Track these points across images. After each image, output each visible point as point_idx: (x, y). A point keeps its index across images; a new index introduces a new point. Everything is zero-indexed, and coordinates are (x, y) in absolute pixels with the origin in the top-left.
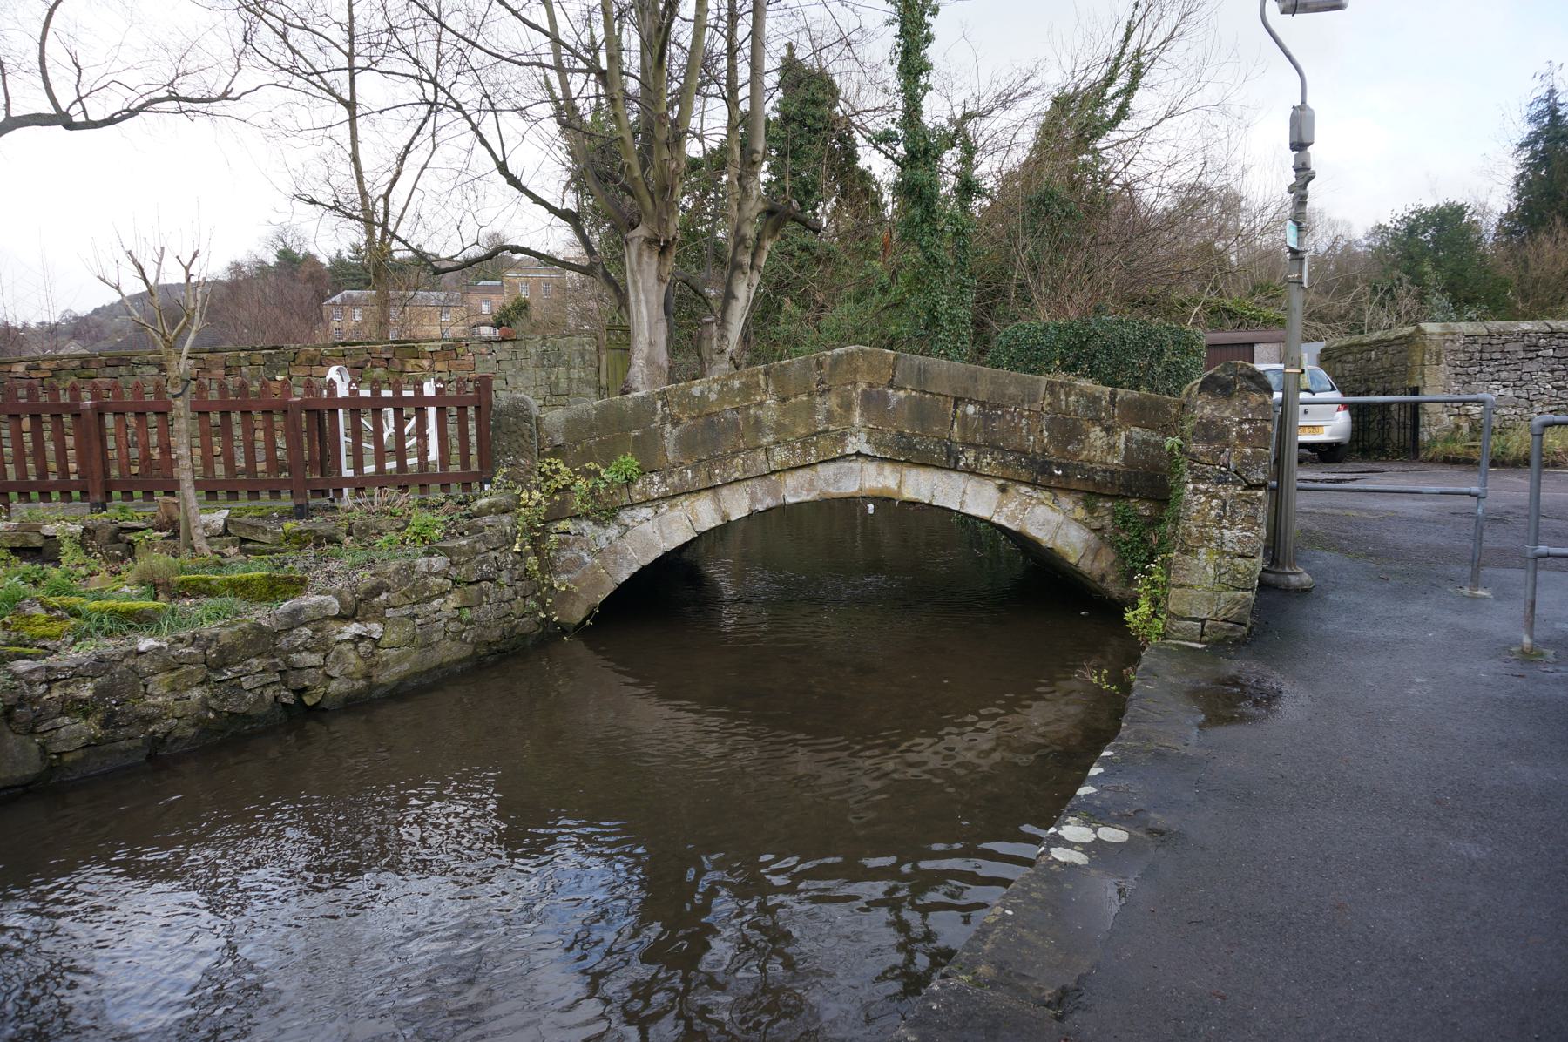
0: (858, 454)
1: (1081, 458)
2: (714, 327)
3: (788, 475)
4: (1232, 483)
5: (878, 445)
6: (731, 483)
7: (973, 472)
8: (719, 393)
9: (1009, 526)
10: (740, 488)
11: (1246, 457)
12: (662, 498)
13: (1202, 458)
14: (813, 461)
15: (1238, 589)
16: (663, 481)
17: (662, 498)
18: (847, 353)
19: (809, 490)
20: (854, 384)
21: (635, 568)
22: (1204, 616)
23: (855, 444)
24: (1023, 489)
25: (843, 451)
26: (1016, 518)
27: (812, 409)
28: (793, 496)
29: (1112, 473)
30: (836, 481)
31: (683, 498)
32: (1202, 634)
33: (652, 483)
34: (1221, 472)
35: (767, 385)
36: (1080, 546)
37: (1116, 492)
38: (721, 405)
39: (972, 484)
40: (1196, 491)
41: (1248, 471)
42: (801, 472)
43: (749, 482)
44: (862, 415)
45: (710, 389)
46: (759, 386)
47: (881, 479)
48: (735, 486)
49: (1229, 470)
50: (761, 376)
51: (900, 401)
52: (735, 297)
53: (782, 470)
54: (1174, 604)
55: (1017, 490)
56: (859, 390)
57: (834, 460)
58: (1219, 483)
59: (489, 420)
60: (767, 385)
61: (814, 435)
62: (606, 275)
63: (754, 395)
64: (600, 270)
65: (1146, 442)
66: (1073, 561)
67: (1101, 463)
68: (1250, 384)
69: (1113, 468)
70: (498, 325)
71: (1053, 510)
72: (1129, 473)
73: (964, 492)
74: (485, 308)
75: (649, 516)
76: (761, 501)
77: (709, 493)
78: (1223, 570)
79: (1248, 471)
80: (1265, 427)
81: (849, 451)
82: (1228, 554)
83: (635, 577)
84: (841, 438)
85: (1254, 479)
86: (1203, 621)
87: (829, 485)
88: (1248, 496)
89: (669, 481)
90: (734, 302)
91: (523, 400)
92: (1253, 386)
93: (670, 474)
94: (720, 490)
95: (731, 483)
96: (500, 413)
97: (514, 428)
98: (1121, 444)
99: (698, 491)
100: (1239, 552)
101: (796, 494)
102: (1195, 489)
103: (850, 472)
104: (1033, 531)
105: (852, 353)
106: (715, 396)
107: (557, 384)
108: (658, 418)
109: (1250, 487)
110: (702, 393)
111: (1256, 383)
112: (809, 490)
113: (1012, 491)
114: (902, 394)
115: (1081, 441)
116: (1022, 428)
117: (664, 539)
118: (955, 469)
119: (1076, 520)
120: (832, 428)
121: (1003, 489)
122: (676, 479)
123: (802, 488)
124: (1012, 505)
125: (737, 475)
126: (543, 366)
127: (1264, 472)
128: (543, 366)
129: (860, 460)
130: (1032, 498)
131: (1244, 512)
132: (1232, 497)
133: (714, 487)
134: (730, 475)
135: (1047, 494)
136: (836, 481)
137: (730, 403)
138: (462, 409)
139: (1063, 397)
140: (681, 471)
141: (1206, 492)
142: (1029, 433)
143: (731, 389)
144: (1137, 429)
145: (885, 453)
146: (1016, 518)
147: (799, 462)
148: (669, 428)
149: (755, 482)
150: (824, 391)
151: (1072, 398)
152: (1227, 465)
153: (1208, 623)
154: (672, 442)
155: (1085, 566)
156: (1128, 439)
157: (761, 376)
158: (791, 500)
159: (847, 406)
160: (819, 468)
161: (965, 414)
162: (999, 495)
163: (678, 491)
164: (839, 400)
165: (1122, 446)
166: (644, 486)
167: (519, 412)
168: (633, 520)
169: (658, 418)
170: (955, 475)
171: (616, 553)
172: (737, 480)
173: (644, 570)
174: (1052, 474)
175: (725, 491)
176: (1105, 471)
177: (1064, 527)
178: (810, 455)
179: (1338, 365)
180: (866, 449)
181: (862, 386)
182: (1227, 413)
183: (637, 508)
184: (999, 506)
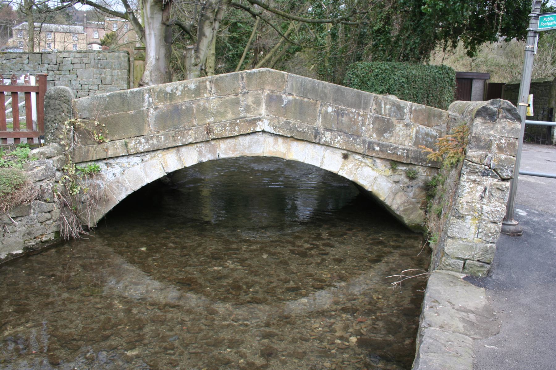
0: (263, 131)
1: (391, 141)
2: (193, 52)
3: (221, 141)
4: (492, 177)
5: (275, 127)
6: (187, 145)
7: (327, 145)
8: (182, 91)
9: (348, 178)
10: (192, 148)
11: (502, 161)
12: (147, 152)
13: (474, 159)
14: (236, 134)
15: (488, 242)
16: (147, 142)
17: (147, 152)
18: (259, 72)
19: (233, 151)
20: (263, 90)
21: (129, 192)
22: (466, 257)
23: (264, 125)
24: (357, 157)
25: (254, 129)
26: (352, 173)
27: (237, 103)
28: (224, 154)
29: (408, 150)
30: (250, 147)
31: (159, 152)
32: (464, 268)
33: (140, 143)
34: (485, 169)
35: (211, 88)
36: (386, 190)
37: (409, 162)
38: (183, 99)
39: (328, 152)
40: (469, 180)
41: (502, 170)
42: (229, 140)
43: (198, 145)
44: (266, 109)
45: (177, 89)
46: (206, 88)
47: (276, 147)
48: (190, 147)
49: (490, 168)
50: (208, 82)
51: (289, 102)
52: (204, 35)
53: (218, 139)
54: (448, 249)
55: (354, 157)
56: (266, 94)
57: (249, 134)
58: (483, 176)
59: (43, 101)
60: (211, 88)
61: (238, 119)
62: (135, 20)
63: (203, 93)
64: (131, 17)
65: (427, 134)
66: (382, 199)
67: (402, 144)
68: (508, 114)
69: (408, 148)
70: (103, 43)
71: (373, 169)
72: (417, 151)
73: (323, 158)
74: (96, 36)
75: (138, 162)
76: (205, 156)
77: (174, 150)
78: (480, 230)
79: (502, 170)
80: (515, 143)
81: (258, 129)
82: (485, 220)
83: (129, 197)
84: (254, 121)
85: (505, 175)
86: (465, 260)
87: (245, 149)
88: (501, 185)
89: (151, 142)
90: (204, 38)
91: (64, 90)
92: (510, 116)
93: (152, 138)
94: (180, 149)
95: (187, 145)
96: (50, 97)
97: (58, 107)
98: (413, 134)
99: (168, 148)
100: (492, 220)
101: (226, 153)
102: (468, 178)
103: (258, 141)
104: (361, 181)
105: (263, 72)
106: (180, 93)
107: (105, 79)
108: (146, 104)
109: (503, 180)
110: (172, 90)
111: (512, 115)
112: (233, 151)
113: (351, 158)
114: (290, 98)
115: (391, 132)
116: (359, 122)
117: (147, 175)
118: (319, 144)
119: (385, 176)
120: (248, 115)
121: (345, 157)
122: (155, 141)
123: (230, 149)
124: (350, 166)
125: (191, 140)
126: (98, 68)
127: (512, 171)
128: (98, 68)
129: (264, 135)
130: (362, 162)
131: (498, 194)
132: (491, 185)
133: (178, 147)
134: (187, 140)
135: (370, 160)
136: (250, 147)
137: (189, 97)
138: (28, 94)
139: (383, 106)
140: (158, 137)
141: (474, 181)
142: (362, 125)
143: (189, 89)
144: (423, 127)
145: (279, 131)
146: (352, 173)
147: (228, 134)
148: (152, 110)
149: (201, 145)
150: (245, 93)
151: (388, 107)
152: (489, 165)
153: (468, 262)
154: (154, 119)
155: (388, 202)
156: (417, 132)
157: (208, 82)
158: (222, 156)
159: (258, 103)
160: (240, 138)
161: (326, 112)
162: (343, 160)
163: (156, 148)
164: (253, 99)
165: (414, 136)
166: (136, 144)
167: (62, 97)
168: (129, 163)
169: (146, 104)
170: (318, 147)
171: (118, 182)
172: (191, 144)
173: (148, 185)
174: (374, 149)
175: (183, 149)
176: (403, 149)
177: (378, 179)
178: (235, 130)
179: (513, 93)
180: (267, 129)
181: (267, 92)
182: (492, 132)
183: (131, 157)
184: (343, 166)
